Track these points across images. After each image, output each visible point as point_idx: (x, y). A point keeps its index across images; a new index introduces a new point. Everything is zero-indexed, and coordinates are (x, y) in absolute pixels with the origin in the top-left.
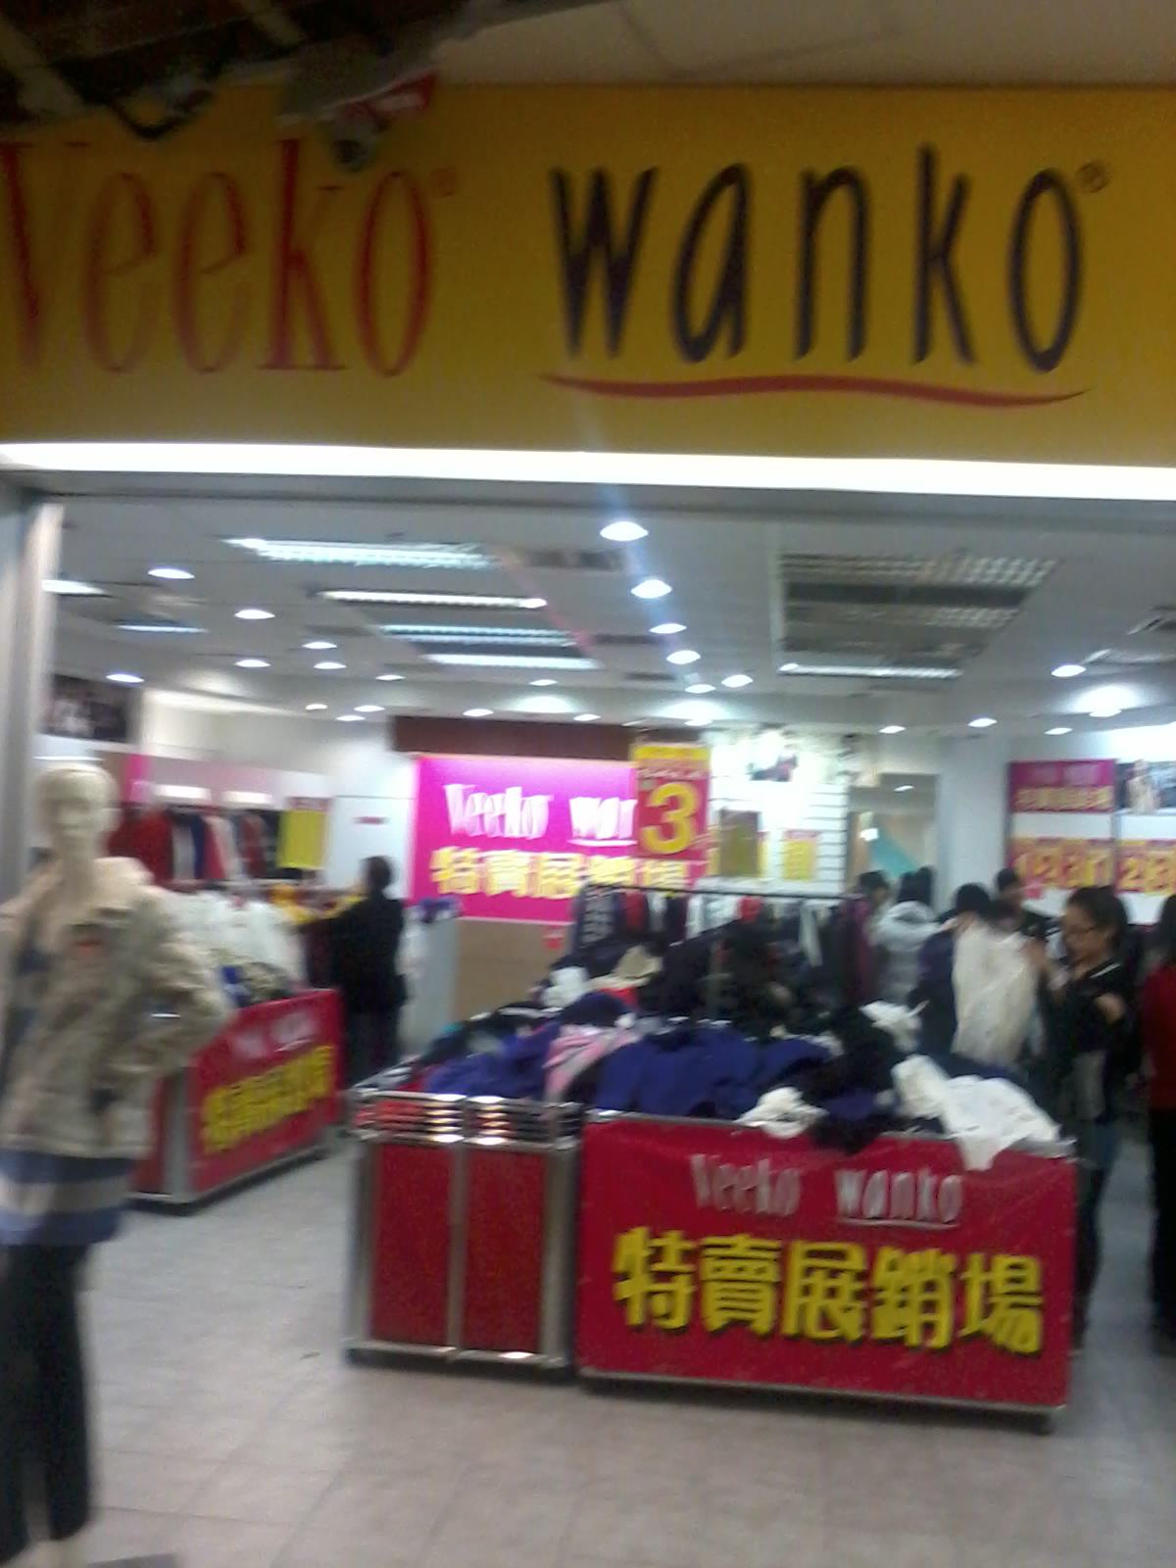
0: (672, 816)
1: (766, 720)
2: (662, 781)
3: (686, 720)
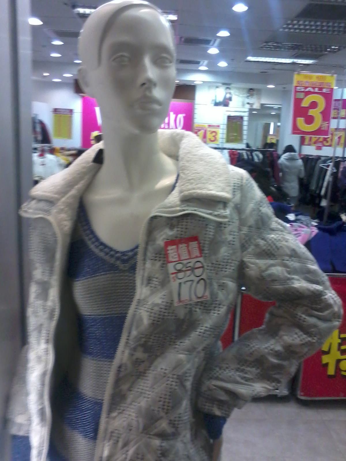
0: (311, 112)
1: (224, 81)
2: (308, 93)
3: (194, 81)
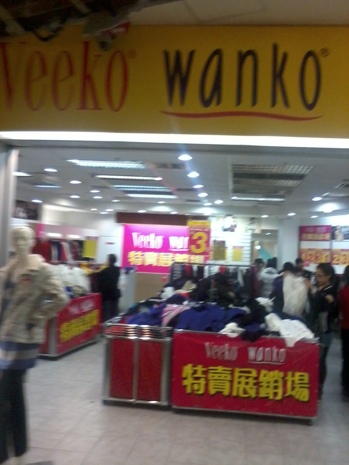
0: (199, 242)
1: (227, 213)
2: (196, 232)
3: (204, 214)
